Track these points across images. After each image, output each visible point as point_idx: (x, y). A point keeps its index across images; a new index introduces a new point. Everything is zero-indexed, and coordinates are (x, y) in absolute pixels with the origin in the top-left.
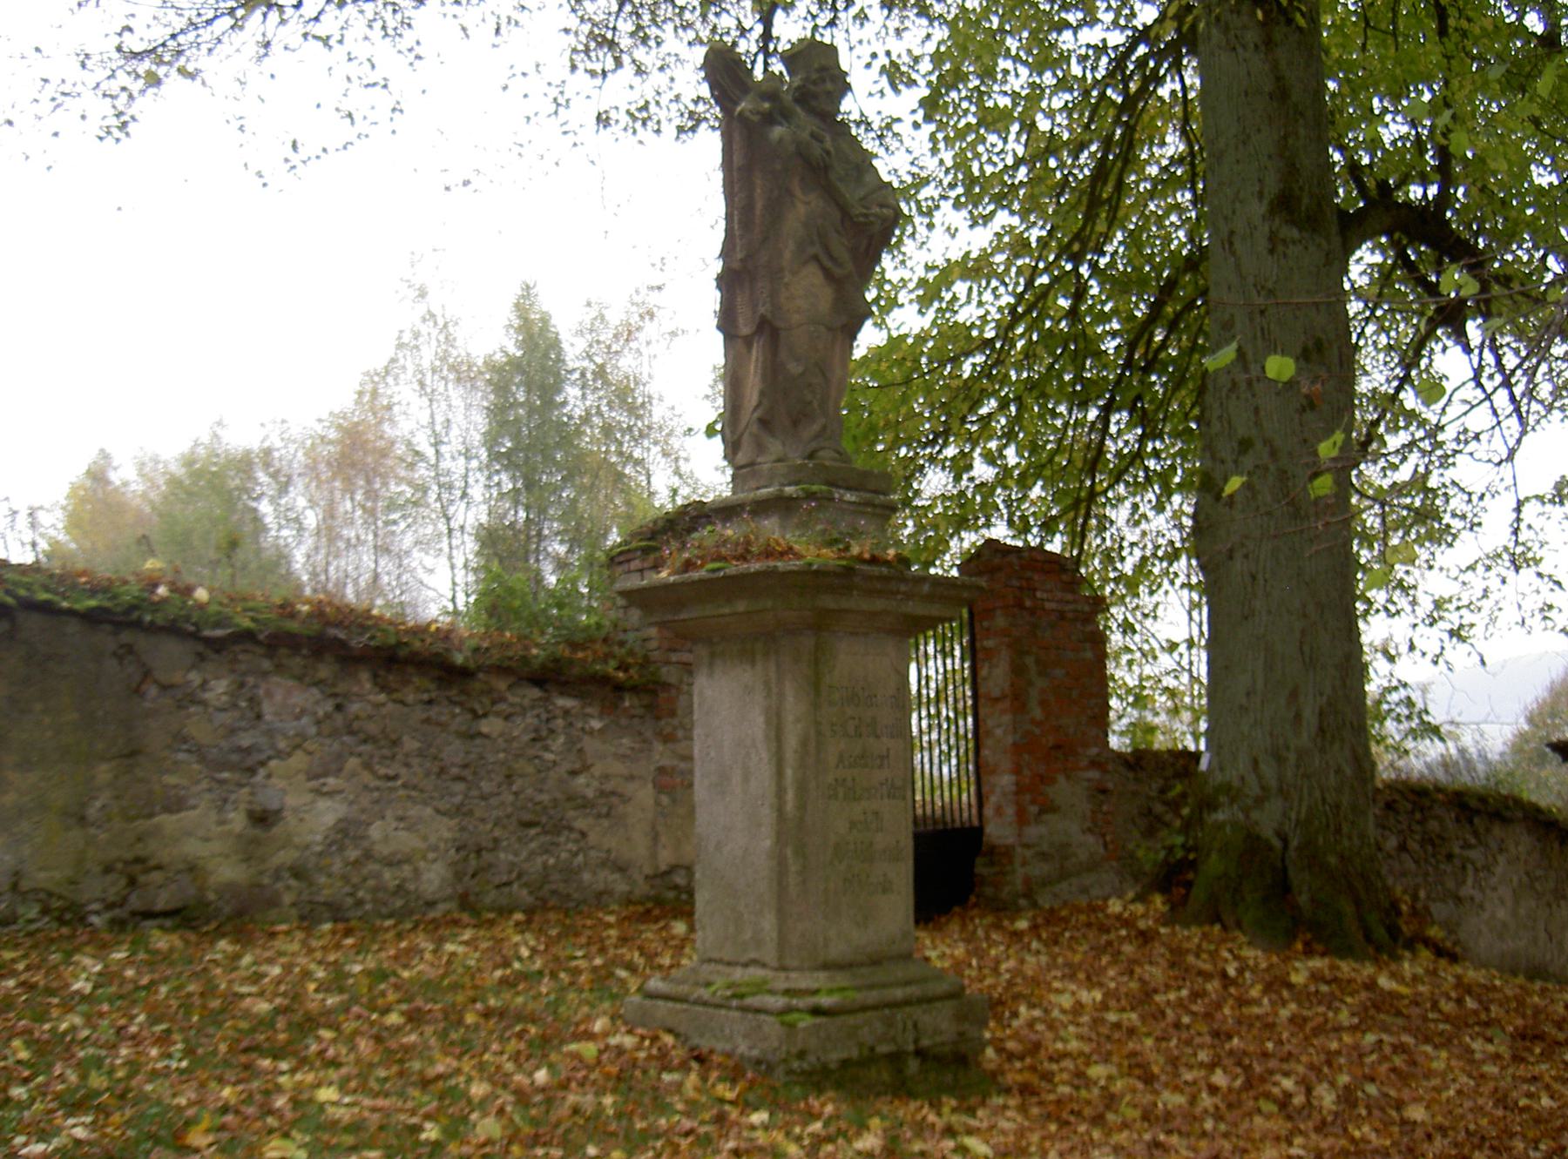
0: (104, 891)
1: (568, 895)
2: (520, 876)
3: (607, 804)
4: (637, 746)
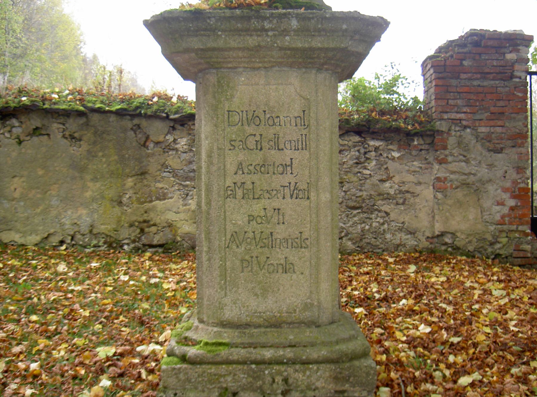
0: (129, 235)
1: (377, 246)
2: (346, 235)
3: (403, 197)
4: (423, 166)
